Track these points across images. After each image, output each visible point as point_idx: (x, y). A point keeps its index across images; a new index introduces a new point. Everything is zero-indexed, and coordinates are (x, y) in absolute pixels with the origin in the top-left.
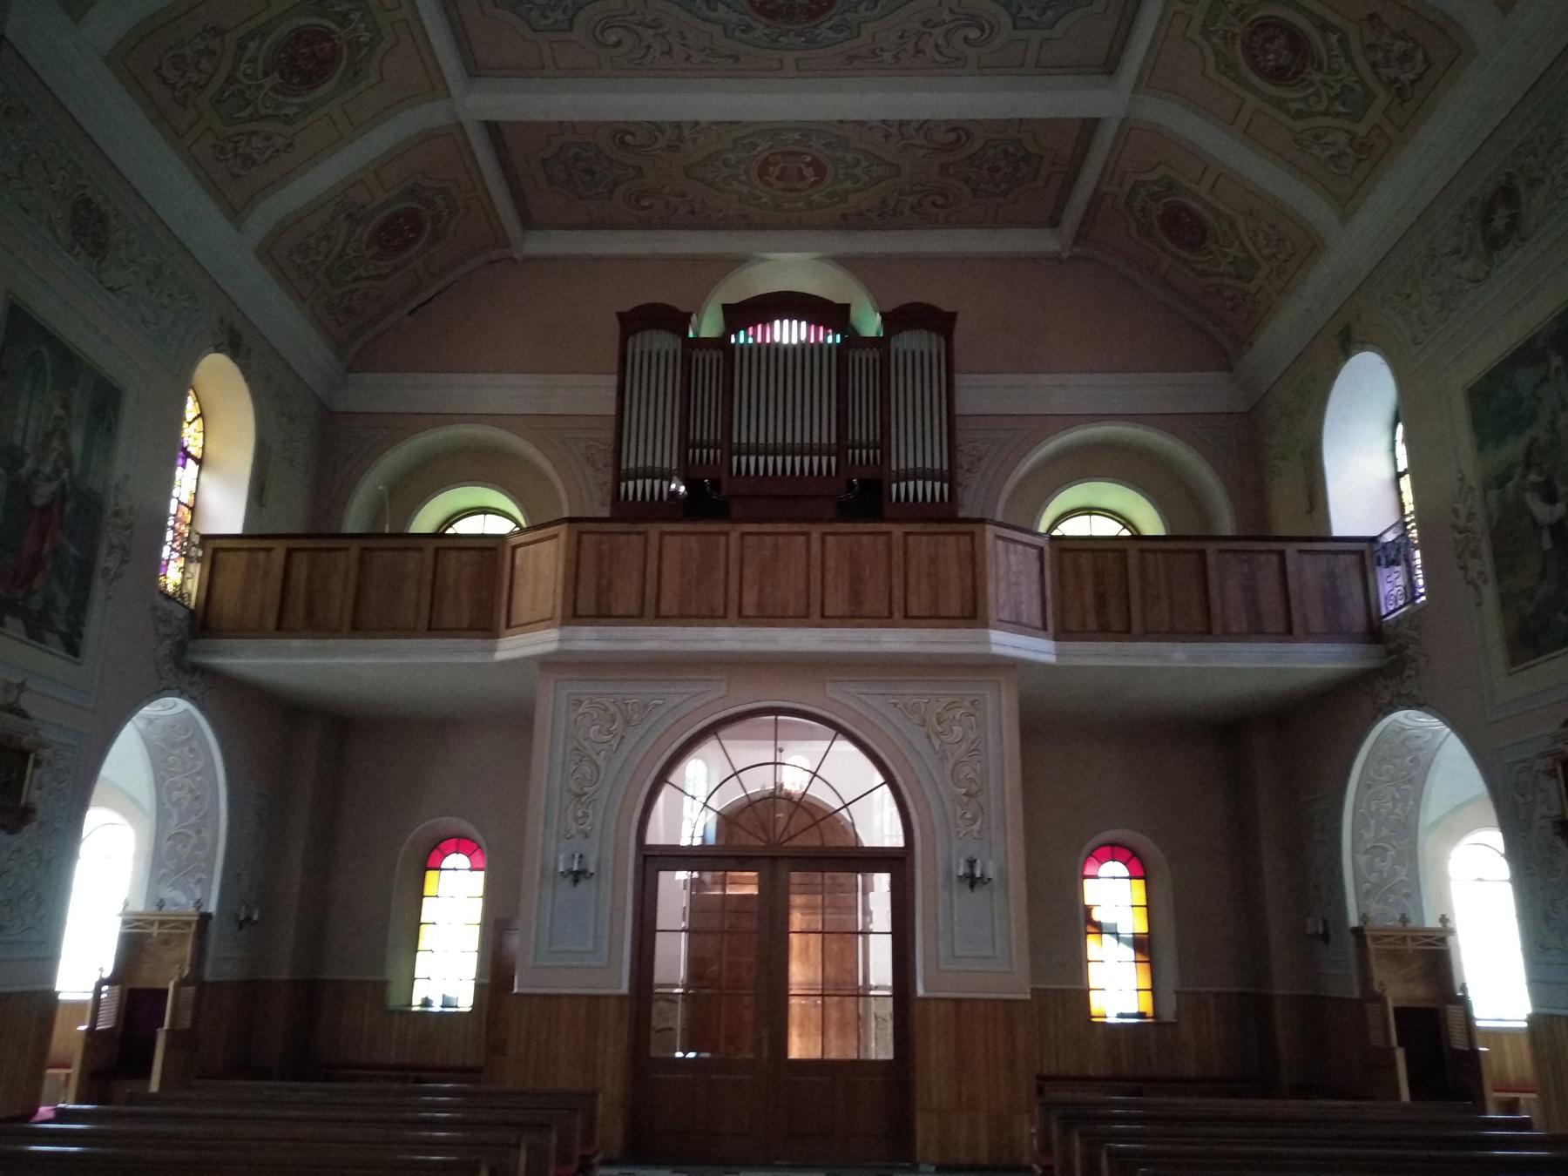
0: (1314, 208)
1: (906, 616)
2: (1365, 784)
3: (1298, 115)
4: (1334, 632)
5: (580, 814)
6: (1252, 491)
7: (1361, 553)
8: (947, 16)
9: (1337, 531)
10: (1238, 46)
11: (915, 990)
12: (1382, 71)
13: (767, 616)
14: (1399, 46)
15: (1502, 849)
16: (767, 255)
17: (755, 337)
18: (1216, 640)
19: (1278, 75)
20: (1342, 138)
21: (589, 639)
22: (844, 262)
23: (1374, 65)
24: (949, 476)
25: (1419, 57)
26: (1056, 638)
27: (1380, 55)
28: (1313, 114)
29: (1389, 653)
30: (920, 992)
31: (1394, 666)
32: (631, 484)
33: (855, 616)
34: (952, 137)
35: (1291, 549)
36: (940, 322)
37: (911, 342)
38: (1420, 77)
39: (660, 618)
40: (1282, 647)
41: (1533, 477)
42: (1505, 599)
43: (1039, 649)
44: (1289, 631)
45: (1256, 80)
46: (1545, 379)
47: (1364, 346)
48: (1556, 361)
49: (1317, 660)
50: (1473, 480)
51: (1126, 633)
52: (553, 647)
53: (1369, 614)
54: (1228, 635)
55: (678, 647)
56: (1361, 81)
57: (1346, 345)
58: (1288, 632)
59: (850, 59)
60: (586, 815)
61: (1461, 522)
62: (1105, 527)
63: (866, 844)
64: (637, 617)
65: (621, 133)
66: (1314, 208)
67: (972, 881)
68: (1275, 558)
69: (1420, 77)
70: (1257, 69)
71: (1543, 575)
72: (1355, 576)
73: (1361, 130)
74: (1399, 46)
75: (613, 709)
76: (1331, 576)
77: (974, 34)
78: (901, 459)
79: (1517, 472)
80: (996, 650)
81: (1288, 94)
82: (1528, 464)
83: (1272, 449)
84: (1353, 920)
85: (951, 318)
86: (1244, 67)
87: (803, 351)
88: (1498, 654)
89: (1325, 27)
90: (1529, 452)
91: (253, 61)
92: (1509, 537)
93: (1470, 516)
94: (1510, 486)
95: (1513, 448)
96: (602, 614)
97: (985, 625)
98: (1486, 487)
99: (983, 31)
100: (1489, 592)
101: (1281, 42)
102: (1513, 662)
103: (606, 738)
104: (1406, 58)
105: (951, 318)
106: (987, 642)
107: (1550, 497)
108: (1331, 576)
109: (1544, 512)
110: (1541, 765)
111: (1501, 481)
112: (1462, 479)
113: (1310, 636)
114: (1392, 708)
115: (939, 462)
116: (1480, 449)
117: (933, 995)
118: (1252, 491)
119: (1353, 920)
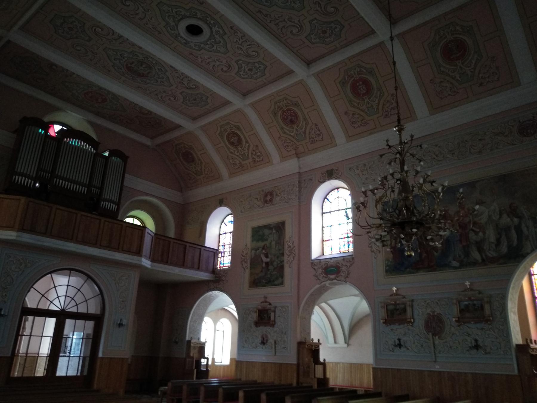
0: (224, 172)
1: (123, 250)
2: (198, 306)
3: (231, 153)
4: (206, 271)
5: (4, 295)
6: (181, 226)
7: (215, 253)
8: (170, 93)
9: (206, 245)
10: (226, 134)
11: (98, 355)
12: (253, 156)
13: (84, 242)
14: (259, 154)
15: (203, 322)
16: (70, 112)
17: (72, 142)
18: (169, 265)
19: (232, 144)
20: (238, 162)
21: (27, 238)
22: (90, 123)
23: (252, 154)
24: (118, 204)
25: (262, 158)
26: (151, 261)
27: (254, 153)
28: (235, 155)
29: (216, 277)
30: (100, 355)
31: (219, 280)
32: (17, 177)
33: (109, 247)
34: (147, 112)
35: (188, 245)
36: (124, 158)
37: (115, 159)
38: (260, 161)
39: (52, 236)
40: (197, 272)
41: (264, 251)
42: (251, 274)
43: (146, 263)
44: (199, 268)
45: (227, 143)
46: (271, 234)
47: (226, 205)
48: (274, 231)
49: (203, 276)
50: (249, 246)
51: (167, 263)
52: (14, 238)
53: (213, 268)
54: (172, 264)
55: (54, 246)
56: (248, 155)
57: (221, 203)
58: (198, 269)
59: (139, 87)
60: (6, 295)
61: (244, 254)
62: (137, 222)
63: (29, 306)
64: (44, 234)
65: (52, 65)
66: (224, 172)
67: (120, 325)
68: (199, 250)
69: (260, 161)
70: (228, 140)
71: (262, 271)
72: (213, 258)
73: (243, 163)
74: (259, 154)
75: (22, 261)
76: (208, 257)
77: (172, 99)
78: (106, 195)
79: (260, 249)
80: (143, 264)
81: (232, 148)
82: (263, 248)
83: (192, 219)
84: (187, 338)
85: (128, 157)
86: (225, 139)
87: (75, 148)
88: (247, 285)
89: (247, 142)
90: (264, 245)
91: (235, 151)
92: (255, 262)
93: (246, 254)
94: (258, 251)
95: (261, 244)
96: (32, 230)
97: (141, 256)
98: (252, 249)
99: (95, 30)
100: (248, 271)
101: (236, 138)
102: (250, 287)
103: (17, 270)
104: (259, 156)
105: (128, 157)
106: (141, 261)
107: (267, 257)
108: (208, 257)
109: (265, 259)
110: (255, 310)
111: (256, 250)
112: (246, 246)
113: (202, 271)
114: (214, 290)
115: (116, 199)
116: (252, 241)
117: (106, 356)
118: (181, 226)
119: (187, 338)
